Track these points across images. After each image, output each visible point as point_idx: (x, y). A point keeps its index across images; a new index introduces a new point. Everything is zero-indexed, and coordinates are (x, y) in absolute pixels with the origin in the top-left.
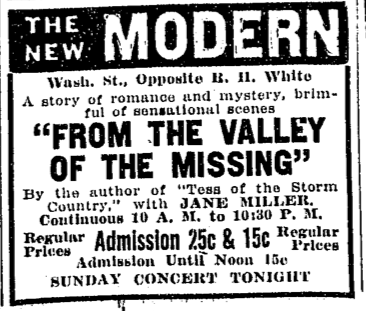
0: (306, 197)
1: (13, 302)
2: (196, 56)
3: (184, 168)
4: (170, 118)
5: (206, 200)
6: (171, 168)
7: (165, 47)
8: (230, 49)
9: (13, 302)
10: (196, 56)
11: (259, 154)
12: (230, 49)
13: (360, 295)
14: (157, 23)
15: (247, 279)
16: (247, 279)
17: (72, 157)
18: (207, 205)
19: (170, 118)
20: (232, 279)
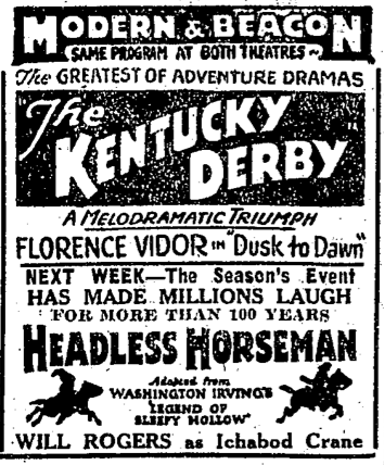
0: (89, 312)
1: (365, 13)
2: (114, 37)
3: (168, 299)
4: (76, 326)
5: (211, 311)
6: (6, 348)
7: (178, 353)
8: (110, 33)
9: (365, 13)
10: (114, 37)
11: (34, 283)
12: (110, 33)
13: (380, 452)
14: (346, 374)
15: (71, 317)
16: (71, 317)
17: (92, 335)
18: (213, 316)
19: (76, 326)
20: (168, 316)
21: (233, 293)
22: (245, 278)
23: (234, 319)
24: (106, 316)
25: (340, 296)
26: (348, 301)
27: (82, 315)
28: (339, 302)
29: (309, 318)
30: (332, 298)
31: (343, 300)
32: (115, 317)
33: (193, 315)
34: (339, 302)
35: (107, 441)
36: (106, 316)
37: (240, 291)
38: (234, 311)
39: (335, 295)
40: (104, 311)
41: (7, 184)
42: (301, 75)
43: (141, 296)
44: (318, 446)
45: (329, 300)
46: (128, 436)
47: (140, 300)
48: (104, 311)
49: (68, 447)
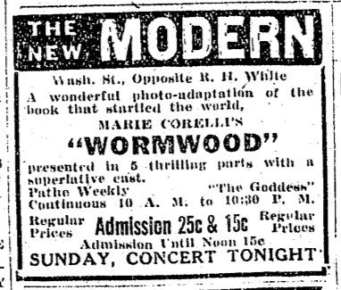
21: (251, 254)
22: (40, 258)
23: (203, 80)
24: (303, 200)
25: (292, 254)
26: (32, 218)
27: (184, 124)
28: (292, 259)
29: (126, 128)
30: (285, 256)
31: (296, 257)
32: (186, 96)
33: (110, 126)
34: (292, 259)
35: (146, 259)
36: (303, 200)
37: (257, 251)
38: (70, 107)
39: (288, 253)
40: (301, 196)
41: (46, 276)
42: (197, 254)
43: (186, 257)
44: (137, 262)
45: (282, 258)
46: (284, 250)
47: (185, 260)
48: (301, 196)
49: (229, 251)
